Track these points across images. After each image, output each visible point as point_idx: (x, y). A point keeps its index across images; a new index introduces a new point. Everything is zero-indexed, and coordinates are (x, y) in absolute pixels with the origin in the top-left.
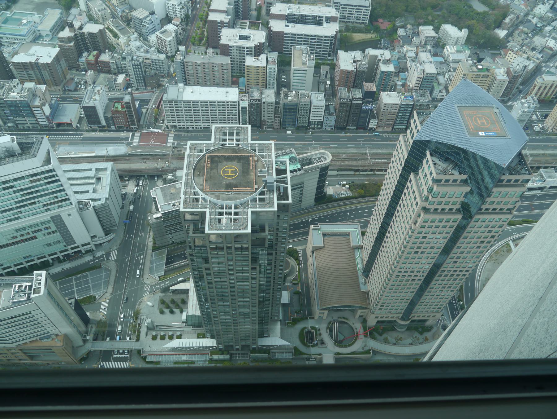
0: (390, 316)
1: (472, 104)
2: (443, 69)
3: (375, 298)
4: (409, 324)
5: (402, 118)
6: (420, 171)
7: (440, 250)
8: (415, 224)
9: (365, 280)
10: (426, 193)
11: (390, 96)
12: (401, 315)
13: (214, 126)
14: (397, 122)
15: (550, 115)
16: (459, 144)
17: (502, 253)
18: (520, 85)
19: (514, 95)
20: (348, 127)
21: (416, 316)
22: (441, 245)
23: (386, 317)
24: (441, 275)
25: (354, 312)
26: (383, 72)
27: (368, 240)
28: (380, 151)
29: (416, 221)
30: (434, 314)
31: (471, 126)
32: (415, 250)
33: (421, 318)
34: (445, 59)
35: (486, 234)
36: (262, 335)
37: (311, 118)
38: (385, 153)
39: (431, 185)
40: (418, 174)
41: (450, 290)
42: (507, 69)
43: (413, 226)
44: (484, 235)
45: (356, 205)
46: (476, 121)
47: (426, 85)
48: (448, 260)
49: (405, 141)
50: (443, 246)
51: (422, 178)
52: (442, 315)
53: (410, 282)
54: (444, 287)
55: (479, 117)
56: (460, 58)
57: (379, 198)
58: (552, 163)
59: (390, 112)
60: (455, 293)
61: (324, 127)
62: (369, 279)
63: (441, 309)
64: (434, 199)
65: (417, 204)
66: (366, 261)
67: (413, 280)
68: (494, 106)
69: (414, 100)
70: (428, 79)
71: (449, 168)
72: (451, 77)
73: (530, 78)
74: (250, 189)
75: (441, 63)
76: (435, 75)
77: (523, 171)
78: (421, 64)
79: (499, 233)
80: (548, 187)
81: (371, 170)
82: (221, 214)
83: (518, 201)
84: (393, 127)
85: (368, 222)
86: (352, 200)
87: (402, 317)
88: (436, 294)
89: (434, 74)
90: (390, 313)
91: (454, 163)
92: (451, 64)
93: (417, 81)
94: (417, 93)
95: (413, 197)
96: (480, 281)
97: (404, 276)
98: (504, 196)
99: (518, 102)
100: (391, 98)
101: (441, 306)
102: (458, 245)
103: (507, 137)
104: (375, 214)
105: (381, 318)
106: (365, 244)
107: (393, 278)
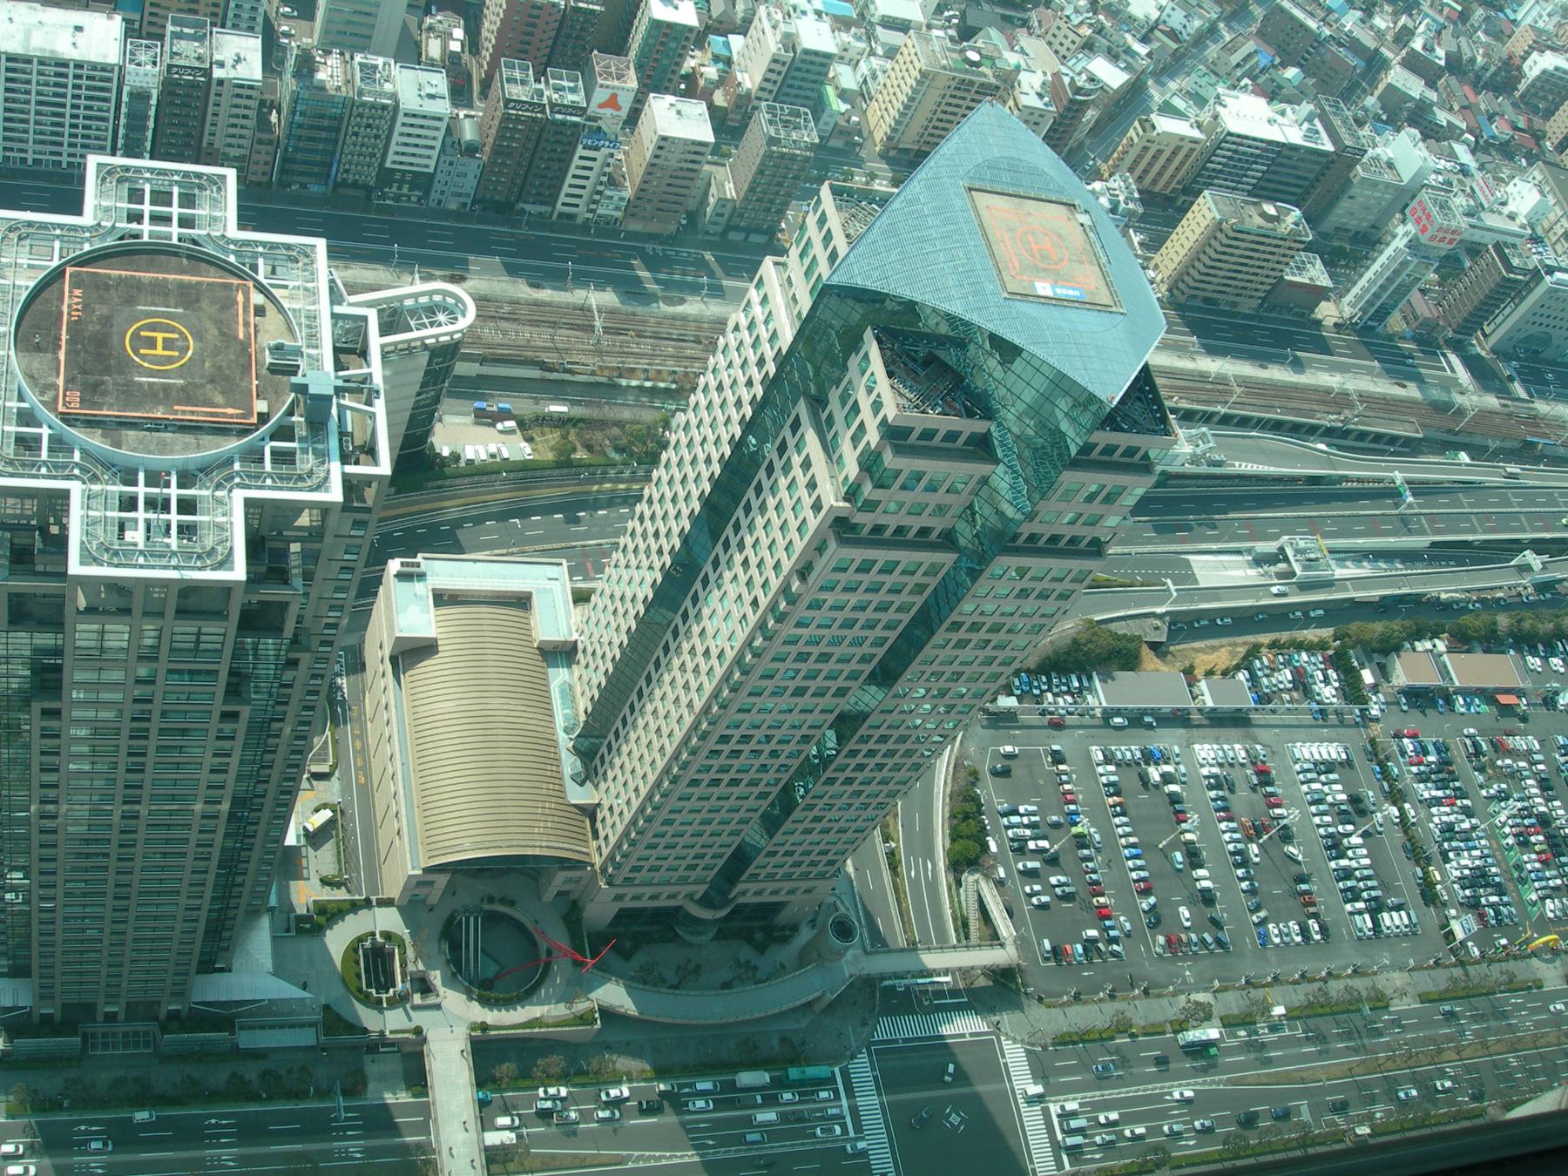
4: (726, 918)
11: (679, 112)
12: (701, 890)
13: (93, 161)
20: (521, 205)
21: (748, 892)
25: (536, 880)
26: (656, 25)
30: (810, 884)
36: (208, 965)
37: (391, 157)
42: (1054, 75)
61: (434, 195)
74: (237, 416)
82: (129, 503)
93: (771, 71)
94: (775, 115)
100: (684, 121)
105: (633, 898)
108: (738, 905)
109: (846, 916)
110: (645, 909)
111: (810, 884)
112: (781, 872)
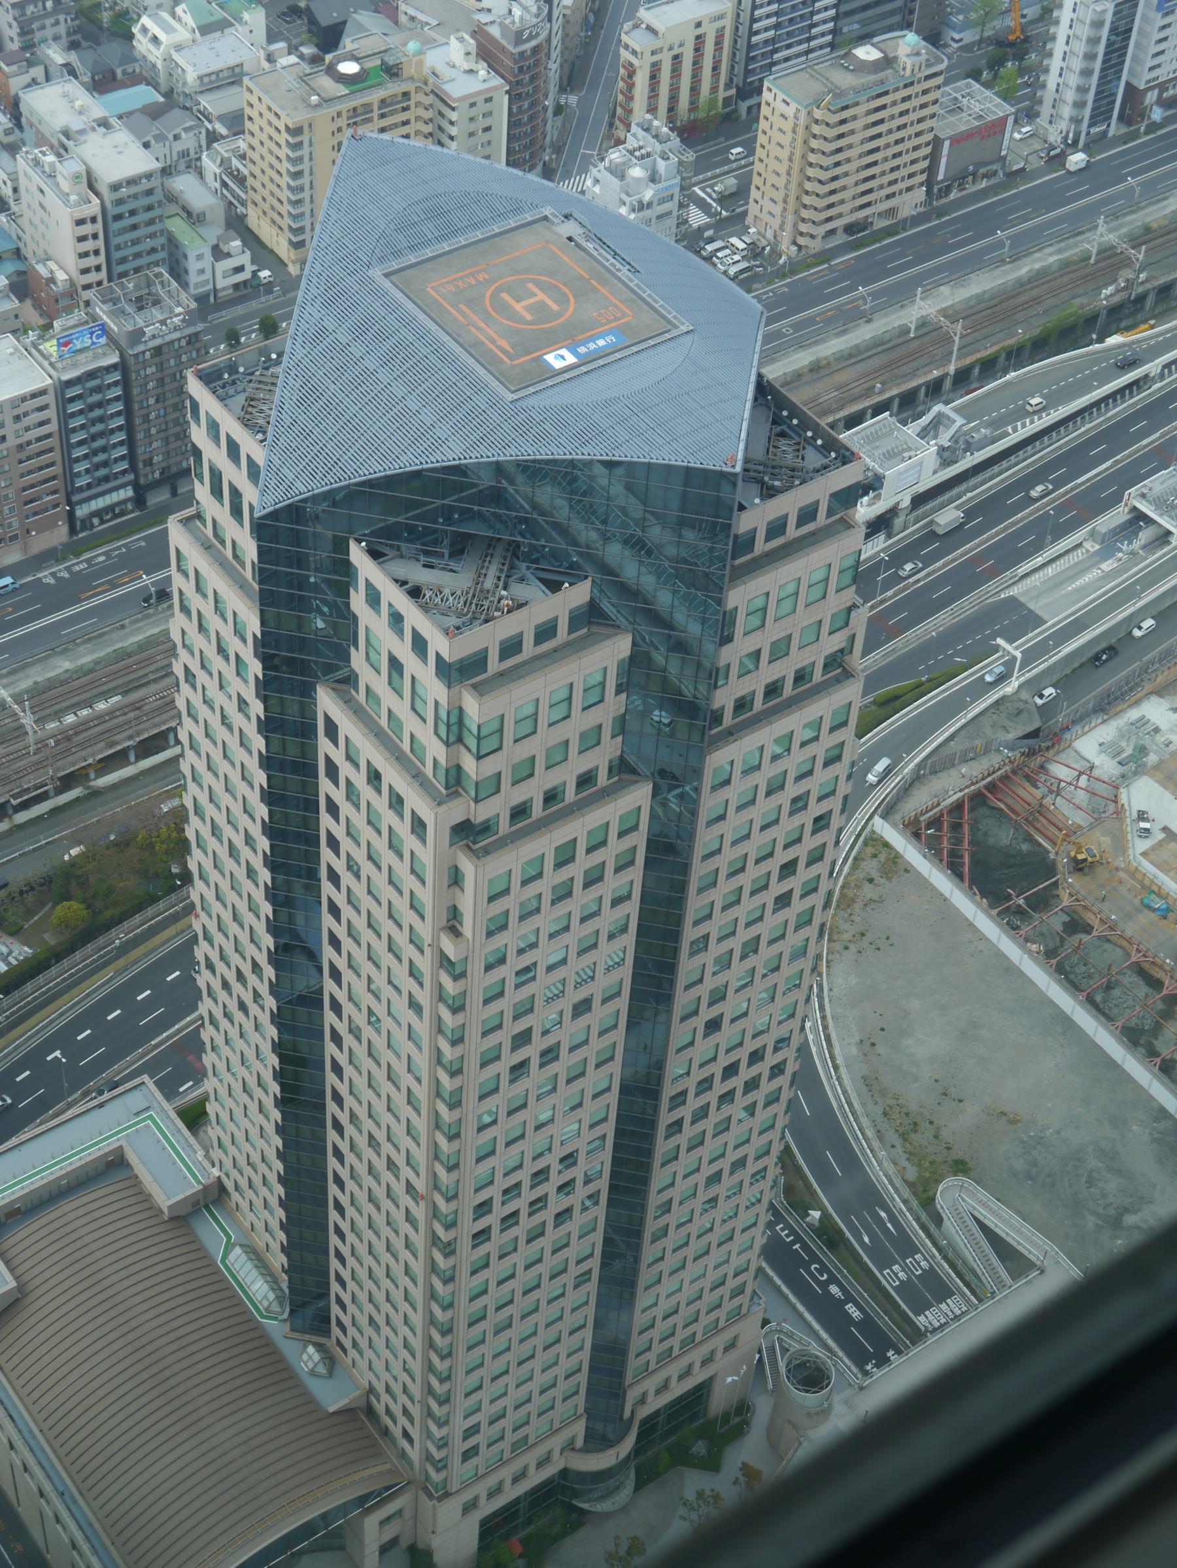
0: (530, 1459)
1: (444, 237)
2: (176, 137)
3: (415, 1411)
4: (638, 1451)
5: (95, 453)
6: (357, 659)
7: (622, 1004)
8: (454, 931)
9: (320, 1347)
10: (436, 750)
12: (579, 1429)
14: (81, 482)
15: (756, 180)
16: (483, 450)
17: (868, 891)
18: (562, 90)
19: (558, 149)
22: (615, 976)
23: (516, 1480)
24: (677, 1125)
25: (342, 1548)
27: (240, 1137)
28: (63, 665)
29: (454, 913)
30: (727, 1336)
31: (493, 341)
32: (511, 1059)
33: (678, 1390)
34: (164, 88)
35: (788, 825)
38: (97, 662)
39: (443, 701)
40: (351, 680)
41: (745, 1174)
42: (474, 34)
43: (449, 947)
44: (779, 833)
45: (77, 995)
46: (503, 308)
47: (135, 242)
48: (679, 1034)
49: (207, 547)
50: (626, 973)
51: (380, 685)
52: (765, 1322)
53: (552, 1235)
54: (716, 1178)
55: (508, 289)
56: (233, 60)
57: (197, 890)
58: (869, 392)
59: (21, 447)
60: (768, 1191)
62: (336, 1331)
63: (749, 1290)
64: (491, 766)
65: (418, 826)
66: (276, 1247)
67: (563, 1216)
68: (547, 211)
69: (113, 342)
70: (133, 213)
71: (488, 584)
72: (235, 163)
73: (588, 46)
75: (153, 113)
76: (155, 182)
77: (813, 459)
78: (61, 151)
79: (841, 793)
80: (906, 502)
81: (67, 782)
83: (854, 606)
84: (71, 515)
85: (193, 1044)
86: (41, 979)
87: (590, 1435)
88: (694, 1229)
89: (149, 176)
90: (522, 1445)
91: (499, 551)
92: (205, 102)
94: (115, 301)
95: (381, 804)
96: (843, 1071)
97: (511, 1219)
98: (787, 606)
99: (594, 171)
101: (739, 1280)
102: (690, 934)
103: (675, 333)
104: (216, 985)
105: (491, 1495)
106: (228, 1163)
107: (467, 1255)
108: (644, 1422)
109: (802, 1353)
110: (517, 1501)
111: (727, 1336)
112: (675, 1342)
